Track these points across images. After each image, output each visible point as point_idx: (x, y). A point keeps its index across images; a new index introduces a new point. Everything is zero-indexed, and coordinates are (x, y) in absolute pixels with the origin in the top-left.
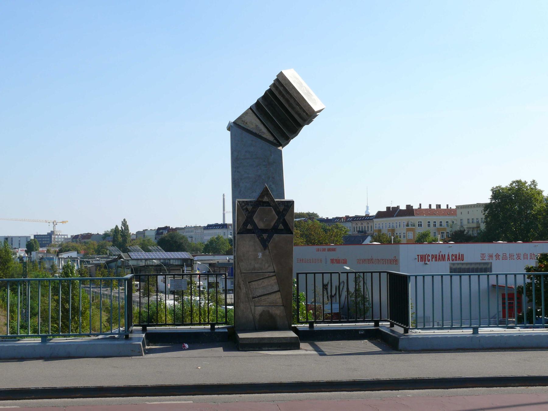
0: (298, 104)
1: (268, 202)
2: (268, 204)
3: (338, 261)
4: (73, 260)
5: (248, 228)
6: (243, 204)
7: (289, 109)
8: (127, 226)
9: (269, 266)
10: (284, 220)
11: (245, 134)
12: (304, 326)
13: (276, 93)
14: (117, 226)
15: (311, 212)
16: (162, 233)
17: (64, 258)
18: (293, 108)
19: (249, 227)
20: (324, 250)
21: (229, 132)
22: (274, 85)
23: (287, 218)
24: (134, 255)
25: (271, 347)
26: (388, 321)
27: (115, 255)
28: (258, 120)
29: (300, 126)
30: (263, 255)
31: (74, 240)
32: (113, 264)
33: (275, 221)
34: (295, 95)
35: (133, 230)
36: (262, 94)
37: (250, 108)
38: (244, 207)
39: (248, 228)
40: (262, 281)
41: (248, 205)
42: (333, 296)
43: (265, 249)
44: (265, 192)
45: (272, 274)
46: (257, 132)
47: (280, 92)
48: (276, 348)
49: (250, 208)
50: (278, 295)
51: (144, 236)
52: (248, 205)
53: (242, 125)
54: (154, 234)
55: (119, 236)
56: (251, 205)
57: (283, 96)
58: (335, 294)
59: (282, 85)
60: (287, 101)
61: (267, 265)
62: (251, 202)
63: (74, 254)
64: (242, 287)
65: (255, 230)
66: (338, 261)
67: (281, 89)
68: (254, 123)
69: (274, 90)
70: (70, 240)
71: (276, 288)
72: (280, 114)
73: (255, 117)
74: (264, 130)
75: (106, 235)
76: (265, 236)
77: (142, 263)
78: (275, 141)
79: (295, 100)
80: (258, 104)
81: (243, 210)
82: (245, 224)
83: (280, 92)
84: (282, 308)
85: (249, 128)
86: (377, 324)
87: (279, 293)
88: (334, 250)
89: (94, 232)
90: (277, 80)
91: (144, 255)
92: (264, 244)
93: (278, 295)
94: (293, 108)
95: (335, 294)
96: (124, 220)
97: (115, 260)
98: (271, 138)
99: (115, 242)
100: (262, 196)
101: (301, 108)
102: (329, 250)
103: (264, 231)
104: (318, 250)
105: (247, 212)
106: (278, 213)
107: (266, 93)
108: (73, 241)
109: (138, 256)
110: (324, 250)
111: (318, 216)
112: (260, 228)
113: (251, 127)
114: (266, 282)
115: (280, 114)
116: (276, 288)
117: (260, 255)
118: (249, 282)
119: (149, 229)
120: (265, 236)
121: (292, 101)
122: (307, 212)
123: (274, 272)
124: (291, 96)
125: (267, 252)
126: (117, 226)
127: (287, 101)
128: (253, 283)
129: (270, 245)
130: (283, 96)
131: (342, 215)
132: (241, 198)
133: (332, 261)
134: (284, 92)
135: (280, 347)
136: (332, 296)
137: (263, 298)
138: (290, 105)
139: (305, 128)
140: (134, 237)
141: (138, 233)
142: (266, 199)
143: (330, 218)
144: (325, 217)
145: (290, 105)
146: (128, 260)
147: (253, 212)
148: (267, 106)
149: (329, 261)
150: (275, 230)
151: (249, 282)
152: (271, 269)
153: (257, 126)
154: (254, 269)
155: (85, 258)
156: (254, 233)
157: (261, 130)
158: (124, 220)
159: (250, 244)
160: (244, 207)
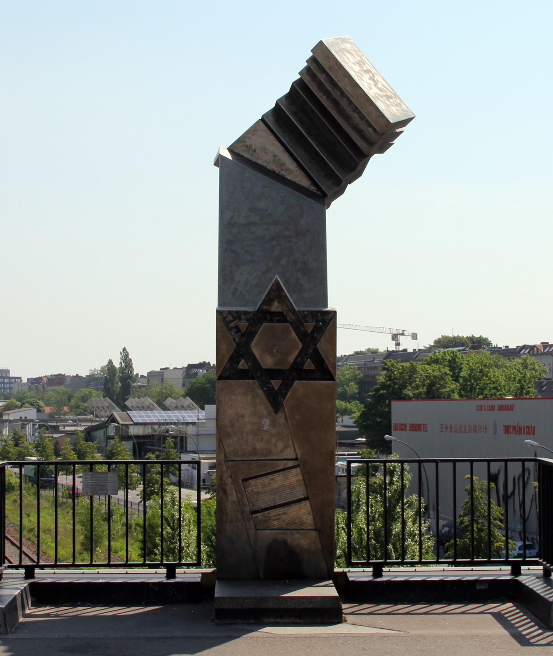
0: (356, 110)
1: (281, 314)
2: (281, 317)
3: (518, 430)
4: (24, 421)
5: (313, 367)
6: (230, 318)
7: (340, 121)
8: (130, 360)
9: (286, 447)
10: (316, 351)
11: (249, 172)
12: (361, 574)
13: (313, 87)
14: (110, 362)
15: (477, 335)
16: (196, 374)
17: (10, 421)
18: (347, 118)
19: (243, 365)
20: (492, 408)
21: (218, 169)
22: (307, 71)
23: (321, 346)
24: (138, 416)
25: (281, 617)
26: (536, 563)
27: (102, 417)
28: (278, 144)
29: (364, 157)
30: (274, 423)
31: (33, 387)
32: (100, 434)
33: (296, 353)
34: (348, 90)
35: (141, 368)
36: (286, 90)
37: (263, 120)
38: (232, 324)
39: (313, 367)
40: (271, 477)
41: (241, 319)
42: (510, 497)
43: (276, 412)
44: (276, 293)
45: (291, 464)
46: (277, 170)
47: (321, 86)
48: (292, 620)
49: (243, 325)
50: (306, 507)
51: (162, 379)
52: (241, 319)
53: (246, 155)
54: (180, 376)
55: (117, 379)
56: (247, 320)
57: (327, 94)
58: (513, 493)
59: (323, 71)
60: (336, 103)
61: (280, 445)
62: (245, 313)
63: (31, 413)
64: (229, 491)
65: (255, 373)
66: (518, 430)
67: (322, 77)
68: (272, 153)
69: (308, 80)
70: (26, 389)
71: (301, 493)
72: (323, 131)
73: (272, 137)
74: (290, 164)
75: (91, 380)
76: (276, 384)
77: (148, 431)
78: (312, 188)
79: (350, 102)
80: (277, 111)
81: (230, 329)
82: (234, 359)
83: (321, 86)
84: (314, 534)
85: (260, 162)
86: (516, 571)
87: (307, 503)
88: (510, 408)
89: (70, 372)
90: (313, 60)
91: (157, 416)
92: (275, 401)
93: (306, 507)
94: (347, 118)
95: (513, 493)
96: (124, 349)
97: (103, 426)
98: (305, 182)
99: (108, 393)
100: (268, 301)
101: (363, 118)
102: (501, 408)
103: (272, 373)
104: (480, 408)
105: (239, 334)
106: (303, 336)
107: (293, 87)
108: (30, 389)
109: (144, 417)
110: (492, 408)
111: (489, 344)
112: (264, 367)
113: (263, 160)
114: (278, 480)
115: (323, 131)
116: (301, 493)
117: (266, 424)
118: (244, 480)
119: (172, 368)
120: (275, 385)
121: (343, 103)
122: (470, 335)
123: (296, 459)
124: (342, 93)
125: (281, 415)
126: (110, 362)
127: (336, 103)
128: (252, 482)
129: (288, 402)
130: (327, 94)
131: (535, 341)
132: (241, 306)
133: (507, 429)
134: (328, 87)
135: (300, 617)
136: (506, 498)
137: (273, 513)
138: (341, 111)
139: (375, 160)
140: (144, 383)
141: (152, 374)
142: (276, 307)
143: (512, 346)
144: (502, 345)
145: (341, 111)
146: (127, 426)
147: (250, 334)
148: (295, 114)
149: (501, 430)
150: (297, 372)
151: (244, 480)
152: (290, 453)
153: (275, 156)
154: (254, 452)
155: (51, 421)
156: (252, 378)
157: (283, 165)
158: (124, 349)
159: (245, 402)
160: (232, 324)
